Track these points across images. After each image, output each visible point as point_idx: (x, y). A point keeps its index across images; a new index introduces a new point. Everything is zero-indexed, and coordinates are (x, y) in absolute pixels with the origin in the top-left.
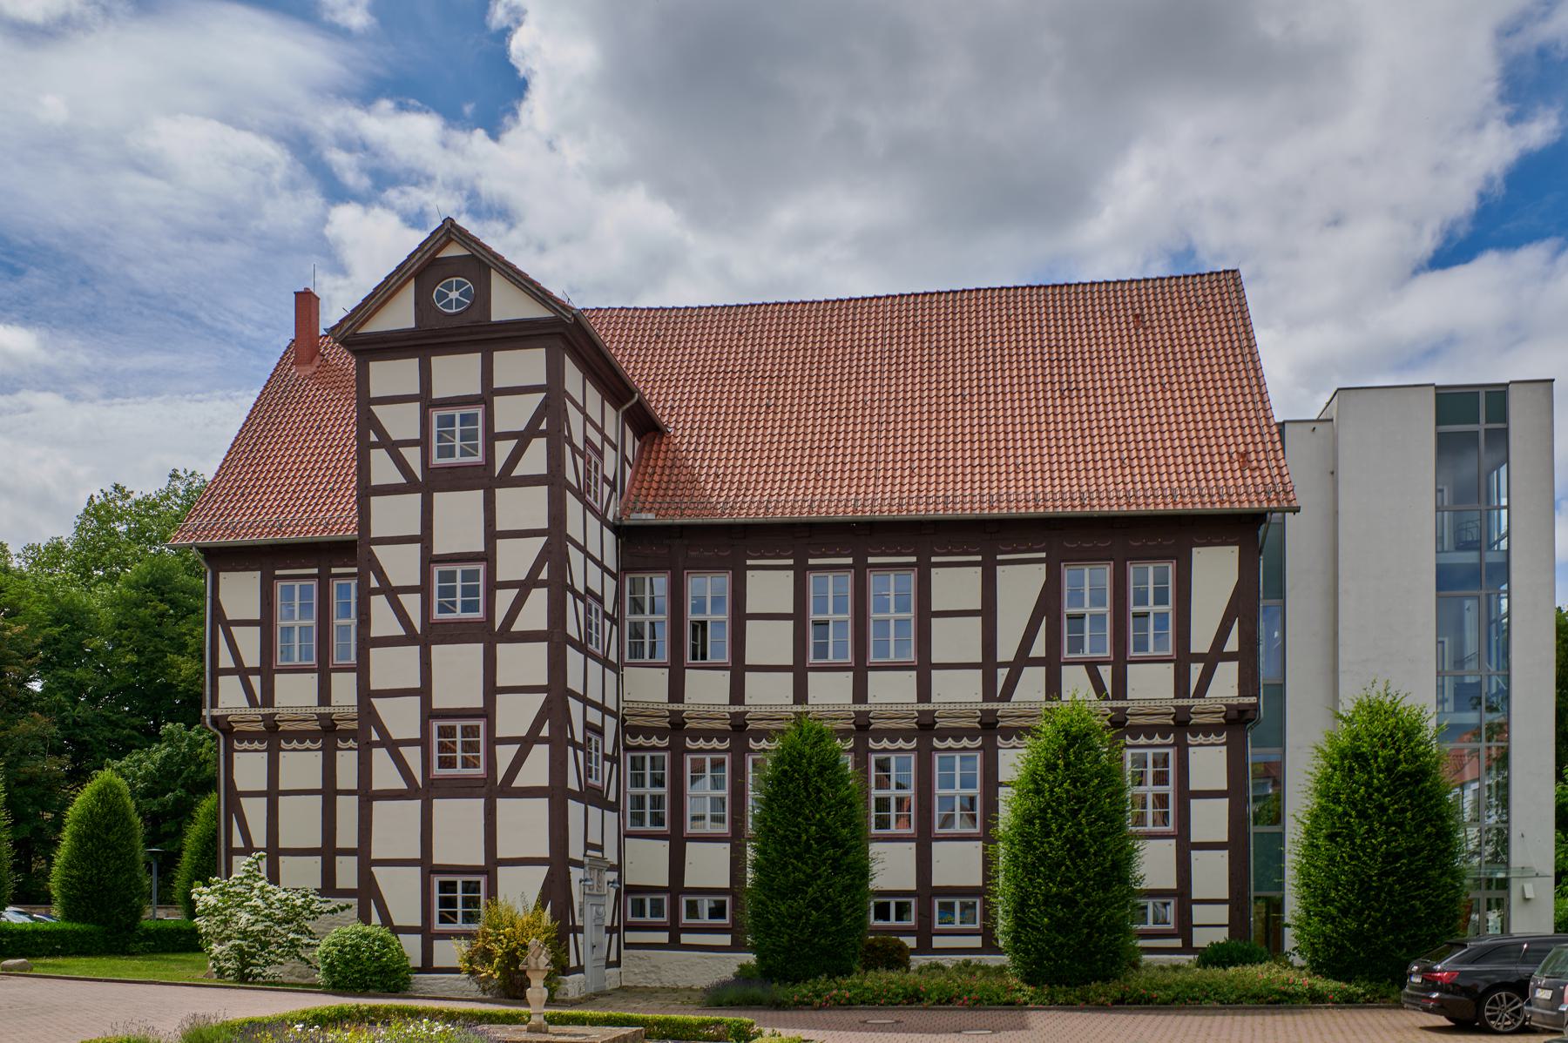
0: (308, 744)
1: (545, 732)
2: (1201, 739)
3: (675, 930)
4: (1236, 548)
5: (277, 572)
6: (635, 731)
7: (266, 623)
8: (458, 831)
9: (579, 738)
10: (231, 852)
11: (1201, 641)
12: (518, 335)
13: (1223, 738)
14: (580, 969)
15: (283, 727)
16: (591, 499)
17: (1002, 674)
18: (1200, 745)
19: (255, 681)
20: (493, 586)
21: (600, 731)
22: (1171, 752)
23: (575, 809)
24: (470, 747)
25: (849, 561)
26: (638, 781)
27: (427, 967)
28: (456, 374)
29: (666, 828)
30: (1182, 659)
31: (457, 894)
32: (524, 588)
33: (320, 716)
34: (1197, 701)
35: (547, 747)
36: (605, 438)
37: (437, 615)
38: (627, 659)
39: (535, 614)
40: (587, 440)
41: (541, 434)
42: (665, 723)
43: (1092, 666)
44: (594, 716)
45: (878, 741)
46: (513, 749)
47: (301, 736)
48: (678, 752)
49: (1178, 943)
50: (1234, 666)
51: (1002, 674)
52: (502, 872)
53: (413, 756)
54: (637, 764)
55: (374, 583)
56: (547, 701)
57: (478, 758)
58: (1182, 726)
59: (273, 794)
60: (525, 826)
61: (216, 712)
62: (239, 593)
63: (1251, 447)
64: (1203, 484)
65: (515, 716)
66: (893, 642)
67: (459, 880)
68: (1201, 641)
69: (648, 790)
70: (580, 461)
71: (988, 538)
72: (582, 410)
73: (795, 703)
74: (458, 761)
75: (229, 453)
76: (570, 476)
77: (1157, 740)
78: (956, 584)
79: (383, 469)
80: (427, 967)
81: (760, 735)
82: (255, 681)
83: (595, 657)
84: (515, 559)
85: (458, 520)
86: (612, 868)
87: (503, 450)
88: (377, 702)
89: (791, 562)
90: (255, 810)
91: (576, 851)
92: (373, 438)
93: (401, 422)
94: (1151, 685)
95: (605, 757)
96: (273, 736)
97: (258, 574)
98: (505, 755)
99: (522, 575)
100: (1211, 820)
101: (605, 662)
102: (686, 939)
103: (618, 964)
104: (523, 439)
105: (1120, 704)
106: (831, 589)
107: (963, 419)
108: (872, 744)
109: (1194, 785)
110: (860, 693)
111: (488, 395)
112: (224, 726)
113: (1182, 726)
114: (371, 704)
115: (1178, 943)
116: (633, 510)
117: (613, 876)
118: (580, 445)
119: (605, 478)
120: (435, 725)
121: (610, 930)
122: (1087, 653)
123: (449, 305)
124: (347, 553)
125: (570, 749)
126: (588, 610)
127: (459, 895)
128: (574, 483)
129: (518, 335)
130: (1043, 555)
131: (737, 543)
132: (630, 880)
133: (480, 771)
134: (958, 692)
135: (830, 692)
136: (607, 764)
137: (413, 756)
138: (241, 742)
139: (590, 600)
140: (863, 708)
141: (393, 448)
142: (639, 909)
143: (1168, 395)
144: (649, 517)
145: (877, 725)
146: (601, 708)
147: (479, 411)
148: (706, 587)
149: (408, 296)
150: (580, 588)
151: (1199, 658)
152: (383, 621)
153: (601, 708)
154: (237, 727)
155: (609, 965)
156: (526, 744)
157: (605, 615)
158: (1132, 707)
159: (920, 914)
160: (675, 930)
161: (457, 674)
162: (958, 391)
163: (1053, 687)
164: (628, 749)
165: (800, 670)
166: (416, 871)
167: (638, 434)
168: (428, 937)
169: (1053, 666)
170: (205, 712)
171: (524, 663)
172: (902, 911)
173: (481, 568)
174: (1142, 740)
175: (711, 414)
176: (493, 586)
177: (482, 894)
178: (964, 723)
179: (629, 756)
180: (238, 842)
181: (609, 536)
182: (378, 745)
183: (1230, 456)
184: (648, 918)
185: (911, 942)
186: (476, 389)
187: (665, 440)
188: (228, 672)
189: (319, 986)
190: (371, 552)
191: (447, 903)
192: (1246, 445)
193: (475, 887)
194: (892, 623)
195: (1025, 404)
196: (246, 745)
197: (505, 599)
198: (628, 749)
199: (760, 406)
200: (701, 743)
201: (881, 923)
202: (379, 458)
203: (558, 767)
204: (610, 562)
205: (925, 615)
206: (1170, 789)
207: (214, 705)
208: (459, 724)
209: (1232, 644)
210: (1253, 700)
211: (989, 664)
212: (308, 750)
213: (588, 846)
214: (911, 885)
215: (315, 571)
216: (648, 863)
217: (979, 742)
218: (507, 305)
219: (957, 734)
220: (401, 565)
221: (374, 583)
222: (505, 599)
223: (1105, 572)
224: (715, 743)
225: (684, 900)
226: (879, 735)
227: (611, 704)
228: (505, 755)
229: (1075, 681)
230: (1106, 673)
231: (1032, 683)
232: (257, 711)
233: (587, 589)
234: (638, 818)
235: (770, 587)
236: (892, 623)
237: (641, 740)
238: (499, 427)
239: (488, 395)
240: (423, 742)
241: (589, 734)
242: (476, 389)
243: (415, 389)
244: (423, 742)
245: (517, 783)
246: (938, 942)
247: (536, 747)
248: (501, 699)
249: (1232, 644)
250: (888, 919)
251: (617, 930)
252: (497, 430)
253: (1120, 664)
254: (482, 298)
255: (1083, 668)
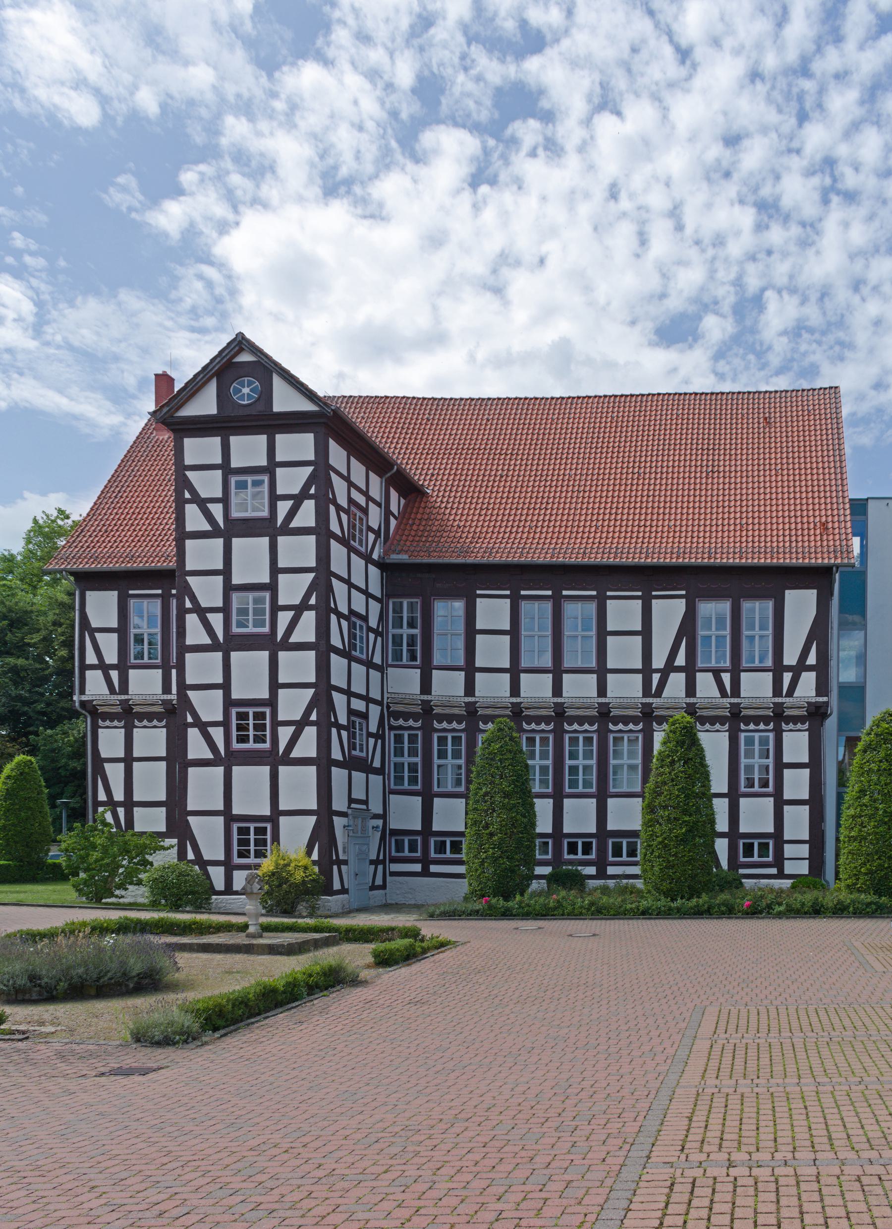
0: (155, 722)
1: (314, 717)
2: (791, 726)
3: (426, 862)
4: (815, 591)
5: (131, 592)
6: (397, 715)
7: (122, 630)
8: (251, 790)
9: (343, 720)
10: (97, 804)
11: (790, 658)
12: (293, 422)
13: (806, 726)
14: (344, 891)
15: (136, 709)
16: (356, 544)
17: (656, 677)
18: (791, 730)
19: (114, 675)
20: (276, 608)
21: (365, 716)
22: (771, 735)
23: (338, 775)
24: (260, 727)
25: (549, 593)
26: (399, 752)
27: (229, 890)
28: (248, 450)
29: (419, 787)
30: (778, 669)
31: (250, 835)
32: (299, 610)
33: (164, 702)
34: (788, 700)
35: (315, 728)
36: (369, 498)
37: (235, 630)
38: (390, 662)
39: (306, 630)
40: (351, 501)
41: (310, 497)
42: (418, 709)
43: (717, 673)
44: (358, 705)
45: (570, 724)
46: (291, 729)
47: (150, 716)
48: (428, 730)
49: (774, 871)
50: (813, 675)
51: (656, 677)
52: (283, 820)
53: (217, 734)
54: (399, 739)
55: (188, 605)
56: (315, 694)
57: (265, 736)
58: (779, 717)
59: (128, 760)
60: (299, 786)
61: (84, 698)
62: (102, 607)
63: (830, 519)
64: (794, 544)
65: (293, 704)
66: (579, 651)
67: (252, 826)
68: (790, 658)
69: (406, 759)
70: (344, 517)
71: (649, 579)
72: (347, 479)
73: (512, 696)
74: (250, 734)
75: (99, 498)
76: (334, 527)
77: (762, 726)
78: (624, 612)
79: (195, 520)
80: (229, 890)
81: (487, 719)
82: (114, 675)
83: (359, 661)
84: (292, 589)
85: (251, 558)
86: (376, 816)
87: (283, 507)
88: (191, 694)
89: (508, 592)
90: (115, 773)
91: (339, 803)
92: (187, 495)
93: (208, 484)
94: (757, 687)
95: (370, 735)
96: (129, 716)
97: (116, 593)
98: (284, 734)
99: (297, 601)
100: (797, 784)
101: (369, 664)
102: (434, 868)
103: (383, 887)
104: (298, 500)
105: (123, 697)
106: (537, 613)
107: (794, 464)
108: (566, 727)
109: (786, 759)
110: (557, 690)
111: (272, 467)
112: (92, 710)
113: (779, 717)
114: (186, 695)
115: (774, 871)
116: (394, 552)
117: (380, 822)
118: (345, 505)
119: (369, 529)
120: (234, 711)
121: (375, 863)
122: (713, 664)
123: (243, 399)
124: (169, 580)
125: (334, 731)
126: (352, 626)
127: (252, 837)
128: (339, 533)
129: (293, 422)
130: (684, 592)
131: (469, 578)
132: (394, 825)
133: (267, 746)
134: (626, 689)
135: (536, 688)
136: (372, 741)
137: (217, 734)
138: (104, 720)
139: (354, 619)
140: (692, 700)
141: (202, 504)
142: (399, 847)
143: (779, 478)
144: (404, 558)
145: (570, 712)
146: (367, 699)
147: (266, 478)
148: (448, 612)
149: (212, 389)
150: (343, 609)
151: (789, 668)
152: (195, 634)
153: (367, 699)
154: (101, 709)
155: (373, 888)
156: (300, 725)
157: (370, 629)
158: (744, 703)
159: (598, 850)
160: (426, 862)
161: (250, 673)
162: (636, 470)
163: (691, 689)
164: (391, 728)
165: (515, 671)
166: (221, 819)
167: (402, 494)
168: (229, 867)
169: (690, 670)
170: (75, 698)
171: (299, 666)
172: (587, 849)
173: (267, 595)
174: (752, 726)
175: (460, 480)
176: (276, 608)
177: (269, 837)
178: (630, 712)
179: (392, 733)
180: (102, 796)
181: (373, 571)
182: (192, 725)
183: (815, 525)
184: (406, 853)
185: (591, 870)
186: (262, 461)
187: (424, 499)
188: (92, 667)
189: (144, 905)
190: (186, 582)
191: (243, 842)
192: (827, 516)
193: (263, 831)
194: (713, 638)
195: (796, 460)
196: (108, 723)
197: (284, 618)
198: (391, 728)
199: (496, 475)
200: (445, 725)
201: (572, 857)
202: (192, 511)
203: (324, 743)
204: (375, 589)
205: (603, 634)
206: (770, 761)
207: (82, 691)
208: (251, 711)
209: (812, 660)
210: (825, 699)
211: (646, 670)
212: (155, 727)
213: (351, 801)
214: (593, 829)
215: (160, 592)
216: (406, 813)
217: (640, 726)
218: (284, 401)
219: (626, 720)
220: (208, 592)
221: (188, 605)
222: (284, 618)
223: (725, 606)
224: (455, 725)
225: (432, 841)
226: (571, 720)
227: (375, 694)
228: (284, 734)
229: (706, 686)
230: (726, 678)
231: (677, 683)
232: (729, 700)
233: (351, 611)
234: (399, 779)
235: (493, 610)
236: (713, 638)
237: (401, 722)
238: (280, 491)
239: (272, 467)
240: (225, 724)
241: (353, 718)
242: (264, 462)
243: (218, 460)
244: (225, 724)
245: (293, 639)
246: (611, 870)
247: (307, 728)
248: (281, 692)
249: (812, 660)
250: (403, 851)
251: (383, 862)
252: (279, 493)
253: (736, 671)
254: (267, 394)
255: (710, 675)
